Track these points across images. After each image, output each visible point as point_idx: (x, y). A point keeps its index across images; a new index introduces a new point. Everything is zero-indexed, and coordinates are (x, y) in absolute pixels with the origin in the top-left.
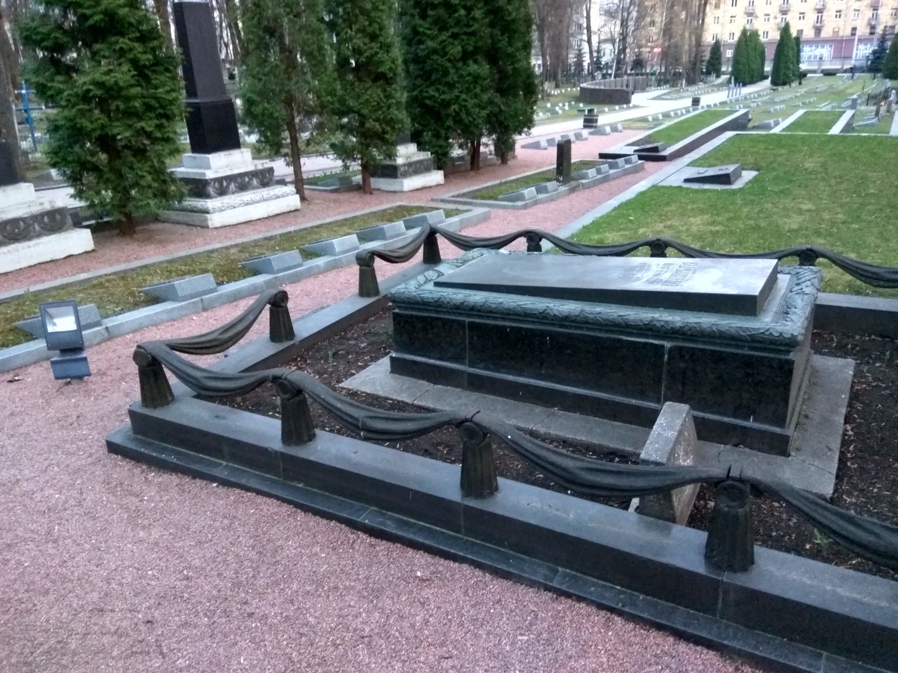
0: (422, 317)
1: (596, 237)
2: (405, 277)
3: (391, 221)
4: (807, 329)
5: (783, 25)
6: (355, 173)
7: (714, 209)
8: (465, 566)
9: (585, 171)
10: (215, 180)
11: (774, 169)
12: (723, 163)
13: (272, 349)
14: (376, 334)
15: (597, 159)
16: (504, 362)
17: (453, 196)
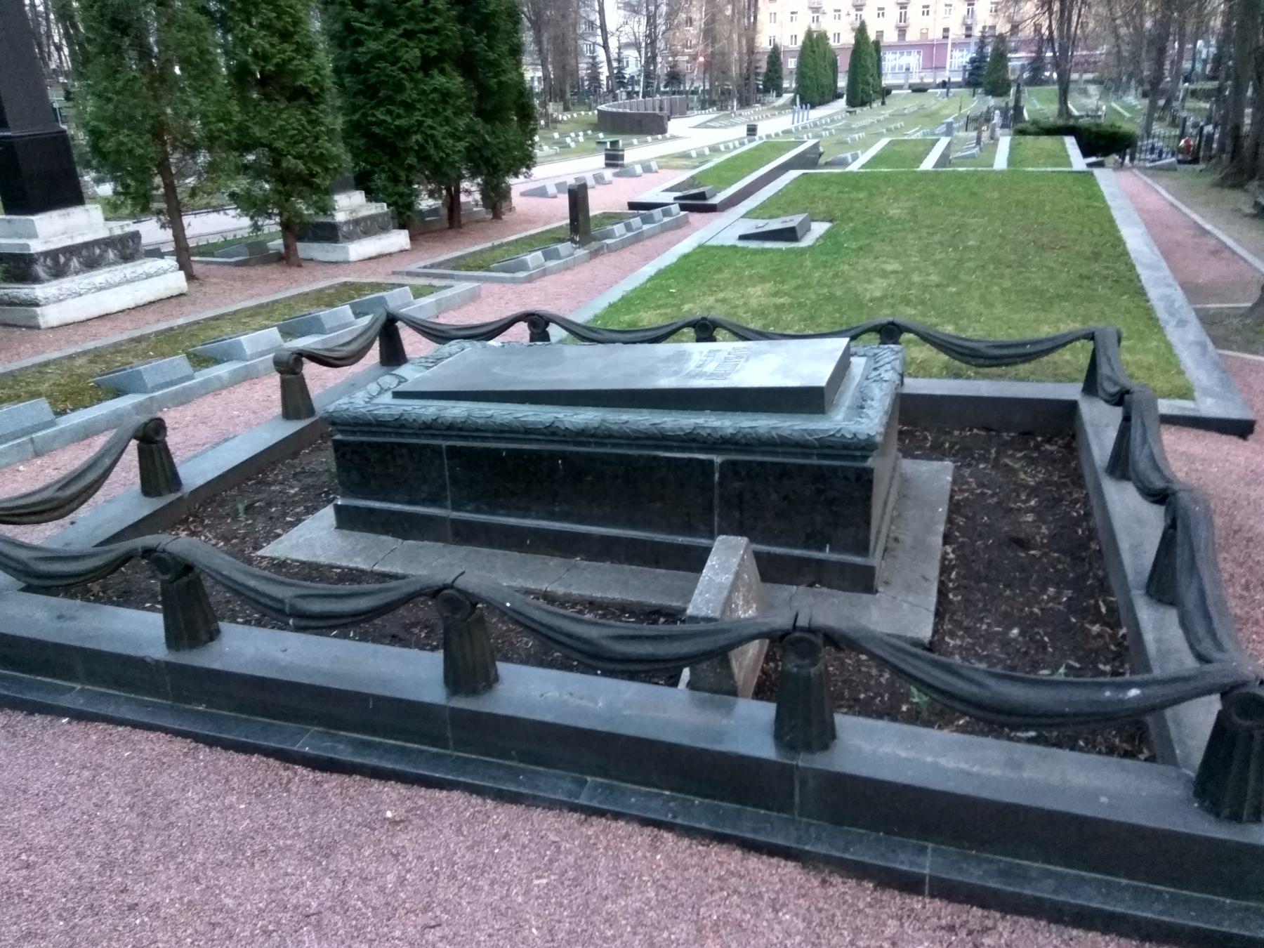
0: (377, 444)
1: (627, 318)
2: (353, 386)
3: (331, 305)
4: (888, 426)
5: (858, 24)
6: (272, 236)
7: (778, 275)
8: (456, 794)
9: (609, 227)
10: (46, 254)
11: (851, 219)
12: (786, 213)
13: (148, 507)
14: (313, 474)
15: (626, 210)
16: (502, 500)
17: (425, 267)
